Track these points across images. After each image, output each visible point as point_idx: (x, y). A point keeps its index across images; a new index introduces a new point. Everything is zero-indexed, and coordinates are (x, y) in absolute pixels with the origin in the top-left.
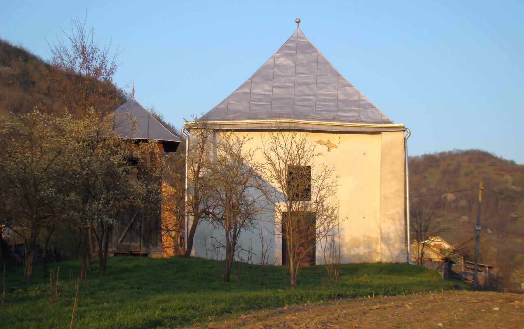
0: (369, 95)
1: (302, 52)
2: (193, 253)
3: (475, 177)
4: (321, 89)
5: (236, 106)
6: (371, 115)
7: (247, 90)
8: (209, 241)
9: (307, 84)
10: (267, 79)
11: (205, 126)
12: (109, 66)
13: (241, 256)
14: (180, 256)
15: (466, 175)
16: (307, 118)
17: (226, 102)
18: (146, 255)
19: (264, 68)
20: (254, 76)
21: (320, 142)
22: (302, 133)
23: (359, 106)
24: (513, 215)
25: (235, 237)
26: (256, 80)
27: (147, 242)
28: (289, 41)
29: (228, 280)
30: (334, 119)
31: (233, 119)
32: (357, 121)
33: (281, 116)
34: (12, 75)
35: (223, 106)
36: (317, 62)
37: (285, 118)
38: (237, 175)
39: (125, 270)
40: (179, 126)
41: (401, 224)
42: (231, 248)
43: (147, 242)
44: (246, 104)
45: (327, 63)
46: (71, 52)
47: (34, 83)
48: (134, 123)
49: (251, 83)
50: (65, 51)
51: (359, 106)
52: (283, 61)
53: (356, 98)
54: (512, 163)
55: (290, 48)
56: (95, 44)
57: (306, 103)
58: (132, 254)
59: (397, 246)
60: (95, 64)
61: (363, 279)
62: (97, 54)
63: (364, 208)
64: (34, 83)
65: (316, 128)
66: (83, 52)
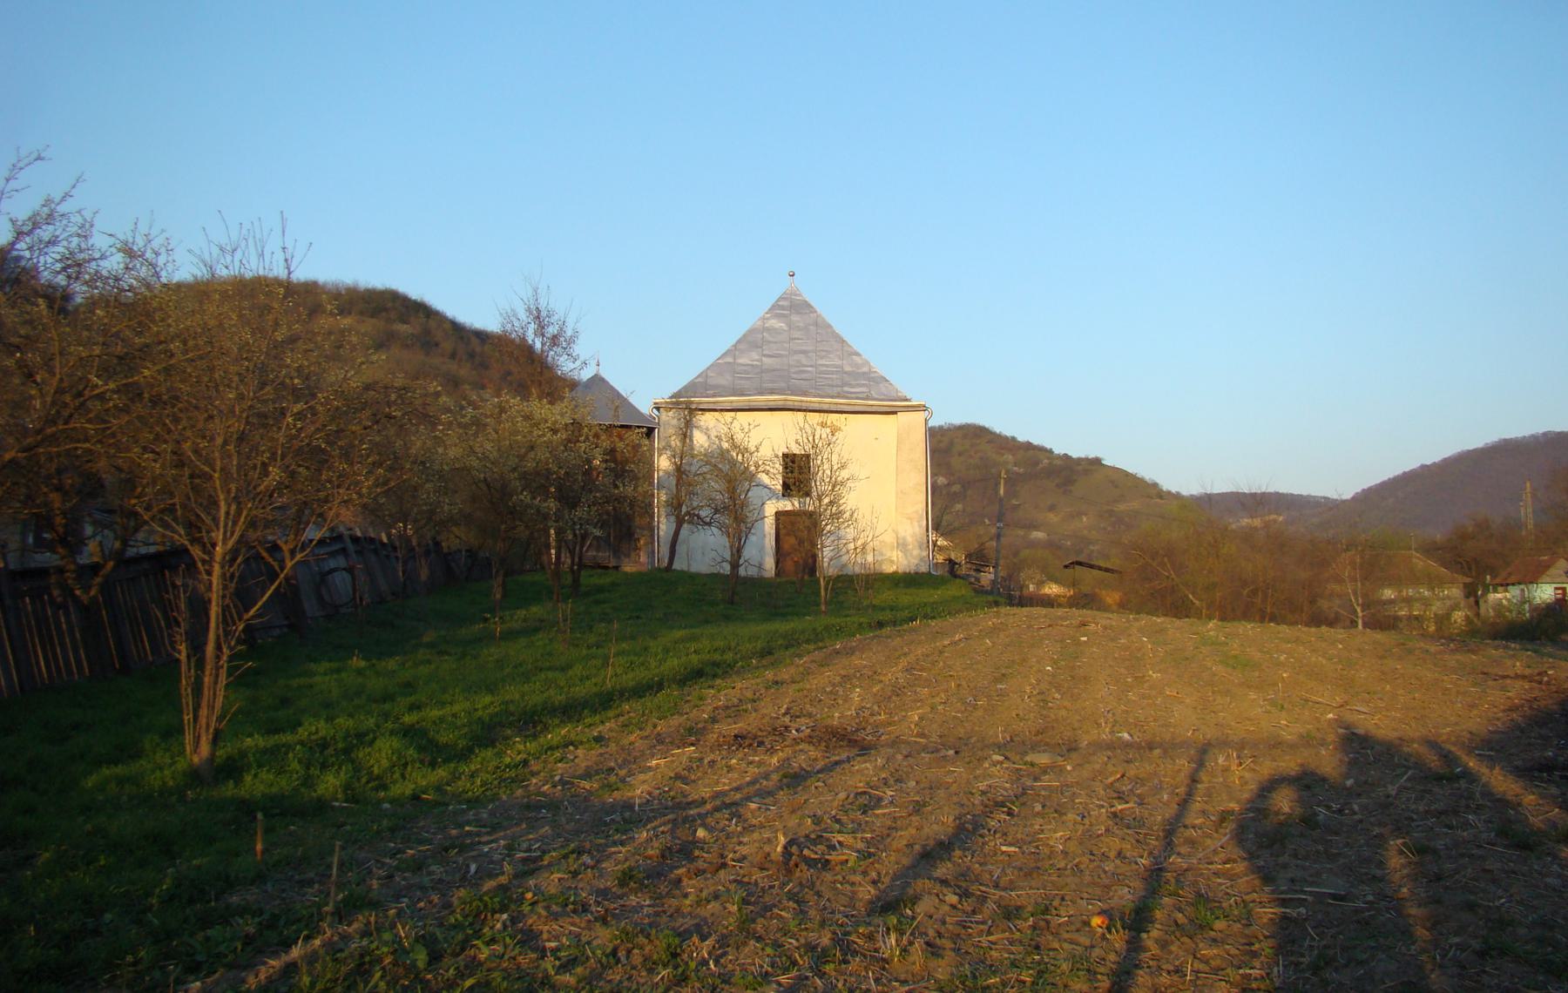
0: (880, 366)
2: (677, 566)
6: (883, 390)
7: (729, 360)
9: (804, 352)
10: (755, 346)
11: (687, 406)
12: (569, 333)
13: (742, 572)
14: (659, 569)
16: (805, 394)
18: (617, 568)
19: (751, 331)
20: (739, 342)
21: (823, 425)
23: (869, 379)
24: (1014, 502)
25: (739, 551)
26: (741, 347)
27: (617, 552)
28: (781, 298)
30: (838, 397)
32: (867, 398)
33: (772, 392)
36: (816, 324)
38: (732, 474)
39: (600, 589)
40: (644, 405)
42: (735, 565)
43: (617, 552)
45: (829, 326)
46: (523, 315)
49: (734, 351)
50: (515, 315)
51: (869, 379)
52: (774, 323)
53: (865, 369)
54: (1014, 439)
55: (783, 308)
59: (916, 552)
60: (552, 330)
61: (886, 596)
63: (883, 511)
64: (437, 345)
65: (817, 406)
66: (539, 318)
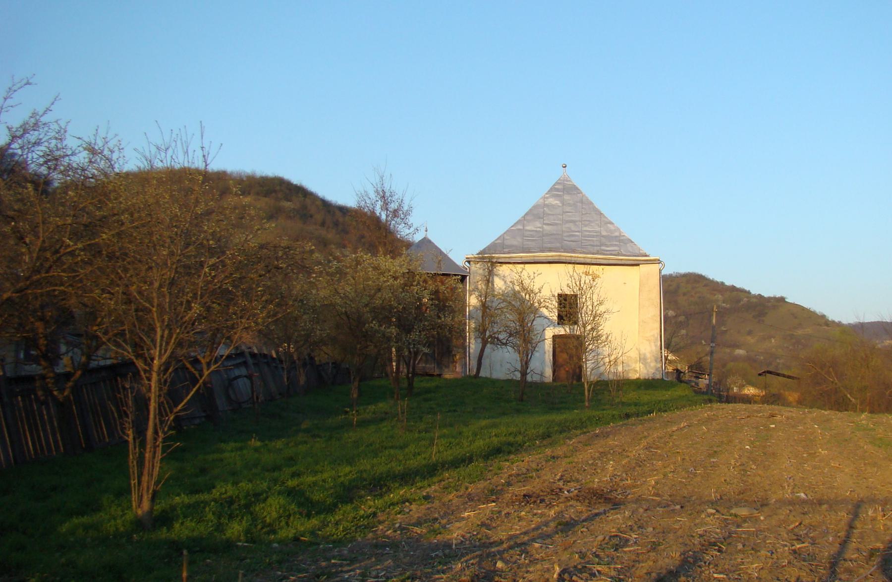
0: (628, 232)
1: (569, 193)
2: (482, 374)
3: (692, 296)
4: (586, 226)
5: (510, 241)
6: (630, 249)
8: (502, 363)
9: (574, 222)
10: (538, 217)
11: (490, 260)
12: (406, 208)
15: (684, 294)
16: (574, 251)
17: (502, 237)
18: (440, 375)
19: (535, 207)
20: (526, 214)
21: (587, 274)
22: (563, 265)
23: (620, 241)
24: (723, 329)
25: (527, 363)
26: (528, 218)
27: (440, 364)
28: (557, 183)
29: (522, 400)
31: (509, 253)
32: (618, 255)
33: (550, 250)
34: (294, 209)
35: (499, 241)
36: (582, 202)
37: (554, 251)
41: (656, 346)
44: (519, 240)
45: (591, 203)
46: (373, 195)
47: (311, 216)
48: (440, 261)
49: (523, 220)
50: (367, 195)
51: (620, 241)
53: (617, 234)
54: (723, 283)
55: (558, 190)
56: (393, 188)
57: (573, 239)
58: (428, 375)
59: (653, 364)
60: (393, 206)
62: (396, 197)
63: (630, 335)
64: (311, 216)
